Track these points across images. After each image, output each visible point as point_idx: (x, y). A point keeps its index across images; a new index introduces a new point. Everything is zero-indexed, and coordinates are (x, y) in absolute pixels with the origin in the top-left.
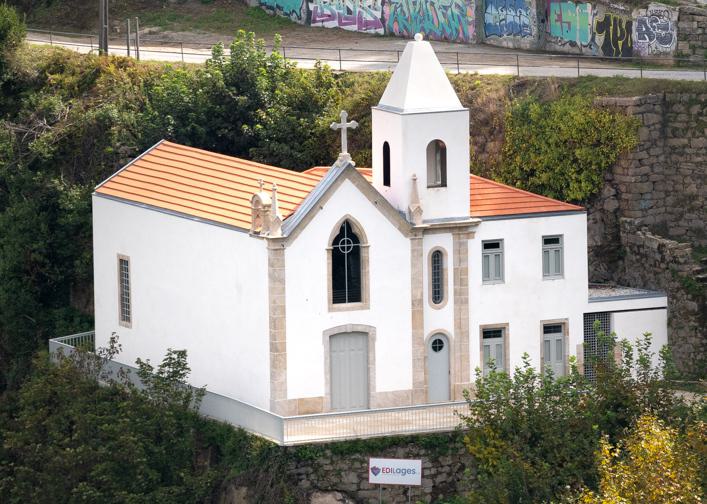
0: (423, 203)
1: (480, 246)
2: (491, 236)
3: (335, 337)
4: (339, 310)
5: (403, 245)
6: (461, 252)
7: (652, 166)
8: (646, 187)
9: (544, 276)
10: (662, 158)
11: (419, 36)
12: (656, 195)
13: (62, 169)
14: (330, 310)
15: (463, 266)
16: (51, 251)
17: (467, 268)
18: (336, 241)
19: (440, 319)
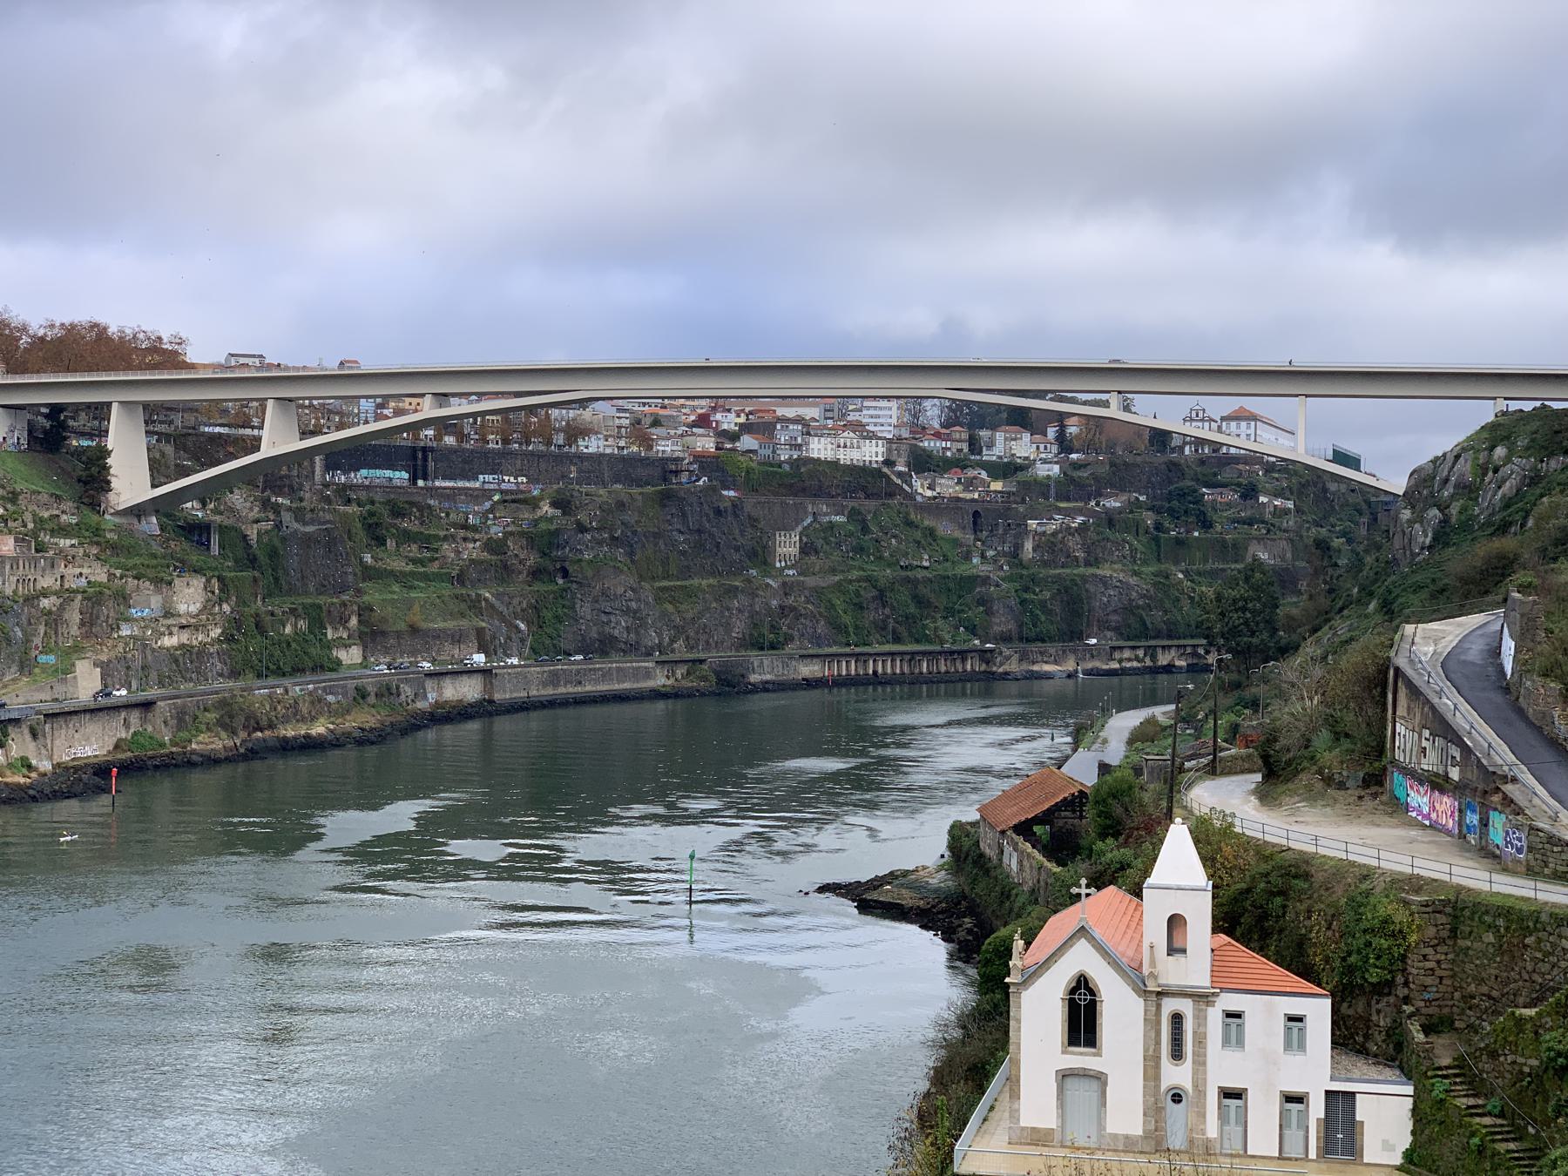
0: (1160, 967)
1: (1220, 1015)
2: (1232, 1008)
3: (1065, 1076)
5: (1137, 1005)
6: (1201, 1019)
7: (1438, 962)
8: (1429, 981)
10: (1450, 956)
12: (1442, 988)
13: (558, 512)
15: (1202, 1029)
18: (1073, 991)
19: (1176, 1075)
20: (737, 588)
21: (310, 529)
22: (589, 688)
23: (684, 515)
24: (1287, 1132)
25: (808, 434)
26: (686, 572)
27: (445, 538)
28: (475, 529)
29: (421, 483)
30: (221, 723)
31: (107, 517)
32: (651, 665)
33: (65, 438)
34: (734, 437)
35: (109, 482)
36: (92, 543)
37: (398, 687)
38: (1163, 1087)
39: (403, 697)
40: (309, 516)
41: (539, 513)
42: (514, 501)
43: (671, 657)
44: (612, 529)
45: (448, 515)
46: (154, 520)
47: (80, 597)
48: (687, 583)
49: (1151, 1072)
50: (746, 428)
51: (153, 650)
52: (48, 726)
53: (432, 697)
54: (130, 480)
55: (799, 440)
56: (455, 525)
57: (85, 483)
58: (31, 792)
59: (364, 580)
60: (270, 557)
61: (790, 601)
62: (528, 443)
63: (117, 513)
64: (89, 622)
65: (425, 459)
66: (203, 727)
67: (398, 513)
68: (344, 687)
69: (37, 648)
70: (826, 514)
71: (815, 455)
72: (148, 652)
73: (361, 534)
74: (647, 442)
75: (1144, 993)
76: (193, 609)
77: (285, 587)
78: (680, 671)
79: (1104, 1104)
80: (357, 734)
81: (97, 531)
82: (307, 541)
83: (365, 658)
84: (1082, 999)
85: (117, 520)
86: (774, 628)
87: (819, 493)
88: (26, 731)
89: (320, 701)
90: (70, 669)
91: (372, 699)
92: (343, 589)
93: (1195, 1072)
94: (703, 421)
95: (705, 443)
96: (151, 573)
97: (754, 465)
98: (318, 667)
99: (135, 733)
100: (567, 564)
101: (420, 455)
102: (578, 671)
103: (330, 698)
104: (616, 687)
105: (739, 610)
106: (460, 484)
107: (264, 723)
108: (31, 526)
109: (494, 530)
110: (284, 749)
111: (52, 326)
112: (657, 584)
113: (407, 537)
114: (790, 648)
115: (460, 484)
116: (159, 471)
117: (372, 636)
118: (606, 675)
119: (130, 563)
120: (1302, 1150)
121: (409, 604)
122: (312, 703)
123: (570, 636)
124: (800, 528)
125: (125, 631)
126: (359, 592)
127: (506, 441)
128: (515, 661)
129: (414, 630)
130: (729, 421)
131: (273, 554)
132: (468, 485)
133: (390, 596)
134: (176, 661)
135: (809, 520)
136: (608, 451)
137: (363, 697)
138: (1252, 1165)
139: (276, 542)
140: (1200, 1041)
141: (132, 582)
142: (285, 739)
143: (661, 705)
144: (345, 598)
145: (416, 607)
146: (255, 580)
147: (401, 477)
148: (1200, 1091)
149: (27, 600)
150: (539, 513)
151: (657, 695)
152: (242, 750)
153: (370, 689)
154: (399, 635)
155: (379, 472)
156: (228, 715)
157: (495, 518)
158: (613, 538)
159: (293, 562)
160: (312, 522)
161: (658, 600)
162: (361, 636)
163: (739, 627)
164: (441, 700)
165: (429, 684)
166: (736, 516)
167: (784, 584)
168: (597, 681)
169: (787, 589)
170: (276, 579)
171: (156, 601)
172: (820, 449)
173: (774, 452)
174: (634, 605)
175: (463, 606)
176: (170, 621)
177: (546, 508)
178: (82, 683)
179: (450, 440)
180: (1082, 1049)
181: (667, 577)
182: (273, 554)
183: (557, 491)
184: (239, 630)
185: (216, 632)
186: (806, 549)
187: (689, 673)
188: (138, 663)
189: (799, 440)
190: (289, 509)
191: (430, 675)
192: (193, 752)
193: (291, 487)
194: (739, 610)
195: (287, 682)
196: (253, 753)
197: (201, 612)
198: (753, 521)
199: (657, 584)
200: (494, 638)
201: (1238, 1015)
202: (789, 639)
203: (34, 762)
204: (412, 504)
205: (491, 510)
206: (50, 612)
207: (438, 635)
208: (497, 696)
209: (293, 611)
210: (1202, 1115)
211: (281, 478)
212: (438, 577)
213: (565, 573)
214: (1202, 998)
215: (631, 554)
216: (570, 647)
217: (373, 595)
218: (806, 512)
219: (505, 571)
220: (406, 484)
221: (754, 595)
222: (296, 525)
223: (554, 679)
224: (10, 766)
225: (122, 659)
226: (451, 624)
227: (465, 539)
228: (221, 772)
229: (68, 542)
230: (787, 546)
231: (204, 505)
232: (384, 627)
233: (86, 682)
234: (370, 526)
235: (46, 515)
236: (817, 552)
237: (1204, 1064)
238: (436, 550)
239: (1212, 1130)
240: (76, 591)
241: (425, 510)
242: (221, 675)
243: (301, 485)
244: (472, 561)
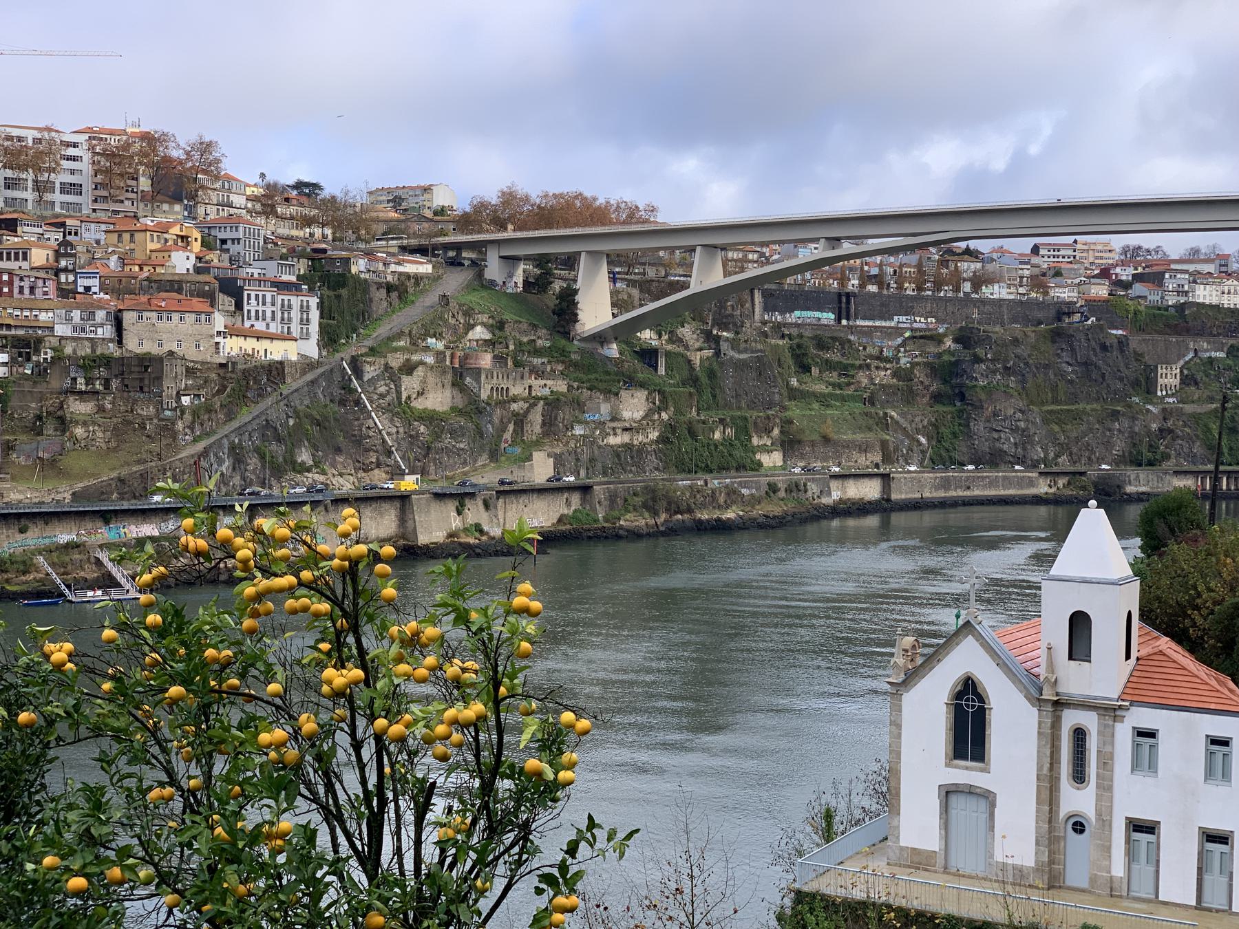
2: (1146, 725)
3: (948, 793)
6: (1108, 737)
9: (1133, 770)
11: (1093, 503)
13: (959, 347)
14: (947, 765)
19: (1077, 800)
21: (743, 356)
23: (1073, 350)
24: (1206, 877)
25: (1195, 282)
26: (1073, 398)
27: (860, 367)
28: (887, 360)
29: (844, 322)
30: (645, 506)
31: (575, 342)
32: (1035, 475)
34: (1126, 286)
35: (576, 315)
36: (558, 362)
37: (805, 485)
39: (809, 494)
40: (743, 346)
41: (943, 347)
42: (921, 337)
43: (1055, 469)
44: (1006, 360)
45: (865, 348)
46: (614, 346)
47: (542, 402)
48: (1073, 407)
51: (600, 447)
52: (501, 501)
53: (836, 495)
54: (596, 310)
55: (1186, 288)
56: (871, 357)
58: (478, 551)
60: (710, 378)
61: (1170, 424)
62: (939, 290)
63: (584, 340)
64: (549, 424)
65: (848, 302)
66: (631, 508)
67: (821, 345)
70: (1206, 351)
71: (1201, 300)
72: (595, 448)
73: (789, 361)
74: (1045, 289)
75: (1038, 702)
76: (638, 415)
77: (721, 402)
78: (1061, 482)
79: (992, 828)
81: (563, 353)
82: (741, 366)
83: (784, 461)
84: (970, 705)
87: (1200, 333)
89: (734, 492)
90: (529, 458)
91: (782, 494)
93: (1099, 798)
94: (1105, 273)
95: (1101, 290)
97: (1142, 308)
98: (740, 467)
99: (575, 511)
100: (964, 390)
102: (968, 478)
103: (745, 491)
104: (1002, 492)
105: (1119, 430)
106: (878, 323)
108: (512, 347)
109: (903, 361)
110: (699, 530)
112: (1046, 408)
113: (829, 366)
114: (1170, 464)
115: (878, 323)
116: (618, 304)
117: (790, 444)
118: (993, 483)
119: (585, 378)
120: (1225, 901)
121: (823, 419)
123: (965, 449)
124: (1182, 363)
125: (579, 431)
126: (784, 408)
127: (920, 288)
128: (913, 468)
129: (826, 440)
130: (1125, 273)
131: (711, 374)
132: (884, 324)
133: (808, 412)
134: (618, 456)
135: (1191, 355)
136: (1012, 297)
137: (774, 492)
138: (1164, 914)
139: (716, 366)
140: (1106, 762)
141: (586, 393)
143: (1043, 510)
144: (769, 412)
145: (829, 421)
146: (691, 394)
147: (828, 317)
148: (1105, 820)
150: (943, 347)
151: (1038, 500)
152: (662, 529)
153: (780, 485)
154: (813, 444)
155: (809, 314)
156: (652, 500)
157: (906, 351)
158: (1006, 368)
160: (745, 351)
161: (1046, 421)
162: (783, 444)
163: (1120, 446)
164: (845, 497)
165: (834, 484)
166: (1122, 351)
167: (1164, 410)
168: (984, 487)
169: (1166, 414)
170: (714, 396)
171: (605, 408)
172: (1205, 294)
173: (1162, 298)
174: (1022, 425)
175: (871, 422)
176: (615, 424)
177: (949, 343)
179: (872, 288)
181: (1056, 401)
182: (711, 374)
184: (673, 434)
185: (654, 435)
186: (1187, 380)
187: (1069, 483)
189: (1186, 288)
190: (727, 339)
192: (621, 527)
193: (735, 325)
194: (1119, 430)
195: (708, 477)
196: (672, 532)
197: (643, 419)
198: (1138, 356)
199: (1046, 408)
200: (896, 449)
201: (1151, 734)
202: (1166, 457)
203: (486, 528)
204: (834, 339)
205: (903, 344)
206: (518, 414)
207: (848, 445)
209: (722, 421)
211: (727, 317)
212: (852, 398)
213: (962, 397)
214: (1110, 712)
215: (1023, 381)
216: (965, 459)
217: (795, 411)
218: (1187, 348)
219: (909, 396)
220: (832, 322)
221: (1134, 419)
222: (732, 353)
224: (466, 530)
226: (859, 437)
227: (877, 368)
228: (642, 545)
229: (540, 361)
230: (1169, 378)
233: (541, 469)
234: (798, 356)
235: (525, 340)
236: (1196, 383)
237: (1110, 789)
238: (853, 377)
239: (1118, 869)
240: (538, 398)
241: (845, 343)
242: (657, 469)
243: (743, 322)
244: (882, 386)
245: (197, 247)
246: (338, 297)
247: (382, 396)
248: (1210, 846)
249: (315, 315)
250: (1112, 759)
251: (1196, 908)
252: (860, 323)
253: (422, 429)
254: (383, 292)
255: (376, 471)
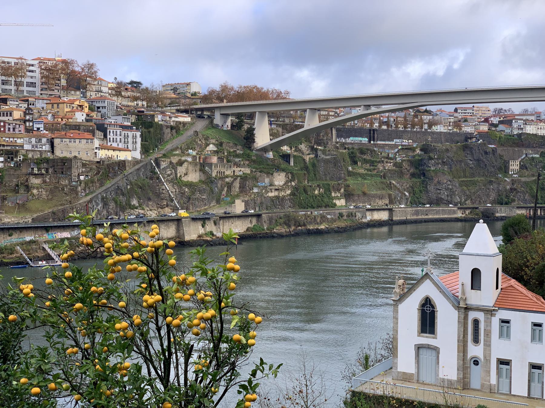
3: (419, 348)
4: (423, 337)
6: (488, 323)
11: (481, 221)
13: (423, 153)
14: (418, 336)
16: (99, 255)
17: (490, 330)
19: (475, 351)
20: (492, 181)
21: (328, 157)
22: (430, 217)
23: (472, 154)
25: (526, 124)
26: (473, 175)
27: (379, 162)
28: (391, 159)
29: (372, 142)
30: (285, 223)
31: (254, 152)
33: (243, 125)
34: (496, 126)
35: (254, 139)
36: (246, 160)
37: (355, 214)
38: (469, 356)
39: (357, 217)
40: (327, 153)
41: (415, 153)
42: (406, 149)
43: (465, 206)
44: (443, 159)
45: (381, 154)
47: (239, 178)
48: (473, 179)
49: (461, 348)
50: (501, 122)
51: (265, 197)
52: (221, 221)
53: (369, 218)
54: (263, 137)
55: (522, 127)
56: (384, 157)
57: (246, 139)
58: (211, 243)
59: (348, 176)
60: (313, 167)
61: (515, 186)
62: (414, 128)
63: (257, 150)
64: (242, 187)
65: (374, 133)
66: (279, 224)
67: (362, 152)
68: (335, 212)
69: (224, 195)
70: (531, 154)
71: (528, 132)
75: (458, 308)
77: (318, 178)
78: (467, 212)
79: (438, 363)
80: (336, 229)
82: (326, 162)
84: (428, 310)
85: (257, 153)
86: (507, 196)
87: (528, 146)
88: (212, 222)
89: (324, 217)
91: (345, 218)
92: (340, 179)
93: (485, 350)
94: (486, 120)
95: (484, 128)
96: (265, 170)
97: (503, 136)
99: (254, 225)
101: (372, 132)
102: (426, 210)
103: (329, 217)
104: (442, 216)
105: (493, 189)
106: (387, 143)
107: (302, 223)
108: (226, 154)
111: (241, 87)
113: (366, 161)
115: (387, 143)
116: (273, 135)
117: (348, 196)
118: (438, 212)
122: (321, 218)
124: (520, 159)
125: (255, 190)
126: (346, 180)
127: (405, 127)
128: (403, 206)
129: (364, 194)
130: (495, 120)
132: (390, 143)
133: (356, 182)
134: (273, 201)
135: (524, 156)
136: (445, 131)
137: (342, 217)
138: (513, 400)
140: (488, 334)
141: (259, 174)
142: (309, 230)
144: (340, 182)
147: (365, 140)
149: (220, 178)
150: (415, 153)
151: (457, 220)
152: (292, 233)
153: (344, 214)
154: (359, 196)
156: (288, 221)
158: (443, 162)
159: (322, 169)
160: (329, 155)
161: (461, 185)
162: (345, 195)
163: (493, 196)
164: (373, 219)
165: (368, 213)
166: (494, 154)
167: (512, 180)
168: (434, 214)
169: (513, 182)
171: (267, 180)
172: (530, 129)
173: (512, 131)
174: (450, 187)
175: (384, 186)
177: (418, 151)
178: (237, 207)
179: (384, 127)
180: (428, 335)
182: (314, 165)
183: (423, 145)
184: (297, 191)
185: (289, 192)
187: (471, 212)
188: (258, 202)
189: (522, 127)
191: (369, 210)
192: (274, 233)
193: (324, 143)
195: (312, 210)
196: (297, 234)
197: (284, 185)
198: (501, 157)
200: (395, 198)
201: (508, 322)
202: (513, 201)
203: (215, 233)
204: (368, 149)
205: (398, 152)
206: (229, 183)
207: (375, 196)
208: (394, 218)
209: (318, 186)
210: (488, 372)
211: (320, 140)
212: (376, 176)
213: (424, 175)
214: (489, 312)
215: (451, 168)
217: (351, 181)
219: (401, 174)
220: (367, 142)
221: (499, 184)
222: (323, 156)
223: (417, 213)
224: (206, 234)
225: (254, 200)
226: (379, 192)
227: (387, 162)
228: (284, 240)
229: (238, 160)
230: (514, 166)
231: (291, 149)
232: (353, 193)
233: (239, 207)
234: (352, 157)
235: (232, 150)
236: (526, 168)
237: (490, 346)
239: (493, 380)
240: (239, 176)
241: (372, 151)
242: (290, 207)
244: (389, 170)
245: (86, 110)
246: (149, 132)
247: (169, 175)
248: (533, 370)
249: (139, 140)
250: (490, 333)
251: (527, 398)
252: (379, 142)
253: (186, 190)
254: (169, 130)
255: (166, 209)
